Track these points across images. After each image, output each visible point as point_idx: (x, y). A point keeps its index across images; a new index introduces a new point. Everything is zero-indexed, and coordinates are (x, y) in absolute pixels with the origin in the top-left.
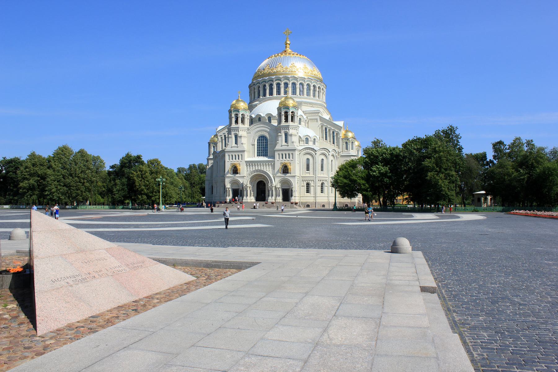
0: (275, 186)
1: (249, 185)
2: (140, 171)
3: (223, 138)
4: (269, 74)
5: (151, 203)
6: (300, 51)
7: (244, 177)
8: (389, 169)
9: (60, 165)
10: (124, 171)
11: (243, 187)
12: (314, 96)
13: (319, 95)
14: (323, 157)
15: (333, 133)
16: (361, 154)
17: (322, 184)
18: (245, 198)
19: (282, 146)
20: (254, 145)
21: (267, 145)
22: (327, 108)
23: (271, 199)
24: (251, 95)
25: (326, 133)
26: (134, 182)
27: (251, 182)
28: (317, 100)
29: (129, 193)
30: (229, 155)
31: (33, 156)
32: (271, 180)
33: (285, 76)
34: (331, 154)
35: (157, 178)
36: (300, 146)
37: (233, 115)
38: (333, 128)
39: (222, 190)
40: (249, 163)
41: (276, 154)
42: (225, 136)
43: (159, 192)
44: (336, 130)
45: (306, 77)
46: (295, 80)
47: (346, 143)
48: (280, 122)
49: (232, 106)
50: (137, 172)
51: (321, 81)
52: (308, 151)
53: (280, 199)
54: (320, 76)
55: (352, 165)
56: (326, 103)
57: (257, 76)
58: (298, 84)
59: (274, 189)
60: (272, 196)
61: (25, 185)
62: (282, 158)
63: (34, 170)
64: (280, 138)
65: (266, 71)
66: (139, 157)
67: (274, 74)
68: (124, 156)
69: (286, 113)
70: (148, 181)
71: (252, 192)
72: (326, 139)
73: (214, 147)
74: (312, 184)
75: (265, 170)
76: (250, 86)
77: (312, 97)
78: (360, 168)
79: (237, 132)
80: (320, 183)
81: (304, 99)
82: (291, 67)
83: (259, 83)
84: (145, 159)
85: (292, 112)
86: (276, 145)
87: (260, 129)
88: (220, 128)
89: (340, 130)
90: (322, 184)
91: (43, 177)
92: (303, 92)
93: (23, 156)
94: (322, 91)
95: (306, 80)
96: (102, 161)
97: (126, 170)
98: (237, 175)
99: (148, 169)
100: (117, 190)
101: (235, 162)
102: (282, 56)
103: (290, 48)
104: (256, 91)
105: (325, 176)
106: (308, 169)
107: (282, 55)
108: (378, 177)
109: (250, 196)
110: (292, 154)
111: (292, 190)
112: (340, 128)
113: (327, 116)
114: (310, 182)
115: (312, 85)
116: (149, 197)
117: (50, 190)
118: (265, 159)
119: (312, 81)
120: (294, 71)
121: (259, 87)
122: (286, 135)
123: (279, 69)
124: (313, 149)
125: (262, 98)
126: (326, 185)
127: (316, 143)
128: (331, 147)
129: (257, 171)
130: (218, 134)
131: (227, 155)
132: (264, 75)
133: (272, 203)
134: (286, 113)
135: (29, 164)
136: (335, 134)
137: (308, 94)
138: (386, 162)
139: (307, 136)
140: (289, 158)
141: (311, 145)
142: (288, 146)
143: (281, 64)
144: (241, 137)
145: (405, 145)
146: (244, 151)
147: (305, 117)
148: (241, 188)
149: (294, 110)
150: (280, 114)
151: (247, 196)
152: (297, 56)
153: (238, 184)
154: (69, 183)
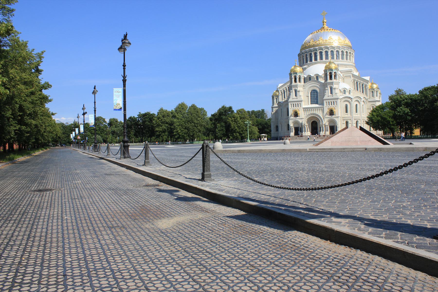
0: (325, 124)
1: (306, 124)
2: (233, 117)
3: (283, 92)
4: (314, 46)
5: (242, 139)
6: (335, 26)
7: (302, 118)
8: (409, 110)
9: (182, 116)
10: (222, 118)
11: (302, 126)
12: (347, 59)
13: (350, 58)
14: (357, 103)
15: (362, 85)
16: (388, 100)
17: (357, 122)
18: (304, 133)
19: (328, 96)
20: (308, 96)
21: (318, 96)
22: (355, 67)
23: (322, 133)
24: (301, 60)
25: (357, 85)
26: (230, 124)
27: (308, 122)
28: (349, 62)
29: (226, 131)
30: (291, 104)
31: (161, 111)
32: (322, 120)
33: (325, 46)
34: (362, 100)
35: (245, 121)
36: (340, 96)
37: (293, 77)
38: (362, 82)
39: (286, 128)
40: (305, 109)
41: (325, 102)
42: (284, 91)
43: (247, 131)
44: (365, 83)
45: (340, 46)
46: (333, 49)
47: (372, 92)
48: (326, 80)
49: (291, 71)
50: (231, 118)
51: (351, 48)
52: (347, 99)
53: (328, 133)
54: (350, 44)
55: (382, 107)
56: (355, 63)
57: (304, 47)
58: (335, 51)
59: (324, 126)
60: (323, 131)
61: (160, 130)
62: (329, 105)
63: (164, 120)
64: (327, 91)
65: (311, 44)
66: (230, 108)
67: (318, 45)
68: (221, 107)
69: (331, 73)
70: (239, 124)
71: (308, 129)
72: (357, 90)
73: (276, 99)
74: (350, 122)
75: (317, 113)
76: (299, 55)
77: (345, 60)
78: (387, 110)
79: (296, 88)
80: (356, 121)
81: (340, 62)
82: (329, 39)
83: (306, 52)
84: (235, 109)
85: (335, 73)
86: (324, 96)
87: (311, 86)
88: (280, 85)
89: (368, 83)
90: (357, 122)
91: (171, 124)
92: (339, 57)
93: (155, 111)
94: (352, 55)
95: (340, 48)
96: (204, 111)
97: (224, 117)
98: (297, 118)
99: (238, 116)
100: (219, 131)
101: (296, 108)
102: (322, 32)
103: (326, 25)
104: (305, 58)
105: (359, 116)
106: (347, 112)
107: (322, 31)
108: (402, 116)
109: (307, 131)
110: (336, 102)
111: (336, 127)
112: (367, 81)
113: (357, 74)
114: (348, 121)
115: (345, 52)
116: (240, 134)
117: (177, 132)
118: (317, 106)
119: (345, 49)
120: (331, 42)
121: (307, 55)
122: (331, 88)
123: (321, 42)
124: (350, 97)
125: (309, 62)
126: (359, 122)
127: (351, 93)
128: (362, 96)
129: (312, 114)
130: (279, 90)
131: (289, 104)
132: (310, 47)
133: (324, 136)
134: (331, 73)
135: (160, 116)
136: (364, 86)
137: (343, 58)
138: (407, 105)
139: (345, 88)
140: (334, 104)
141: (347, 94)
142: (333, 96)
143: (322, 38)
144: (299, 91)
145: (421, 92)
146: (302, 101)
147: (342, 75)
148: (300, 126)
149: (336, 71)
150: (326, 75)
151: (305, 131)
152: (333, 31)
153: (298, 124)
154: (189, 127)
